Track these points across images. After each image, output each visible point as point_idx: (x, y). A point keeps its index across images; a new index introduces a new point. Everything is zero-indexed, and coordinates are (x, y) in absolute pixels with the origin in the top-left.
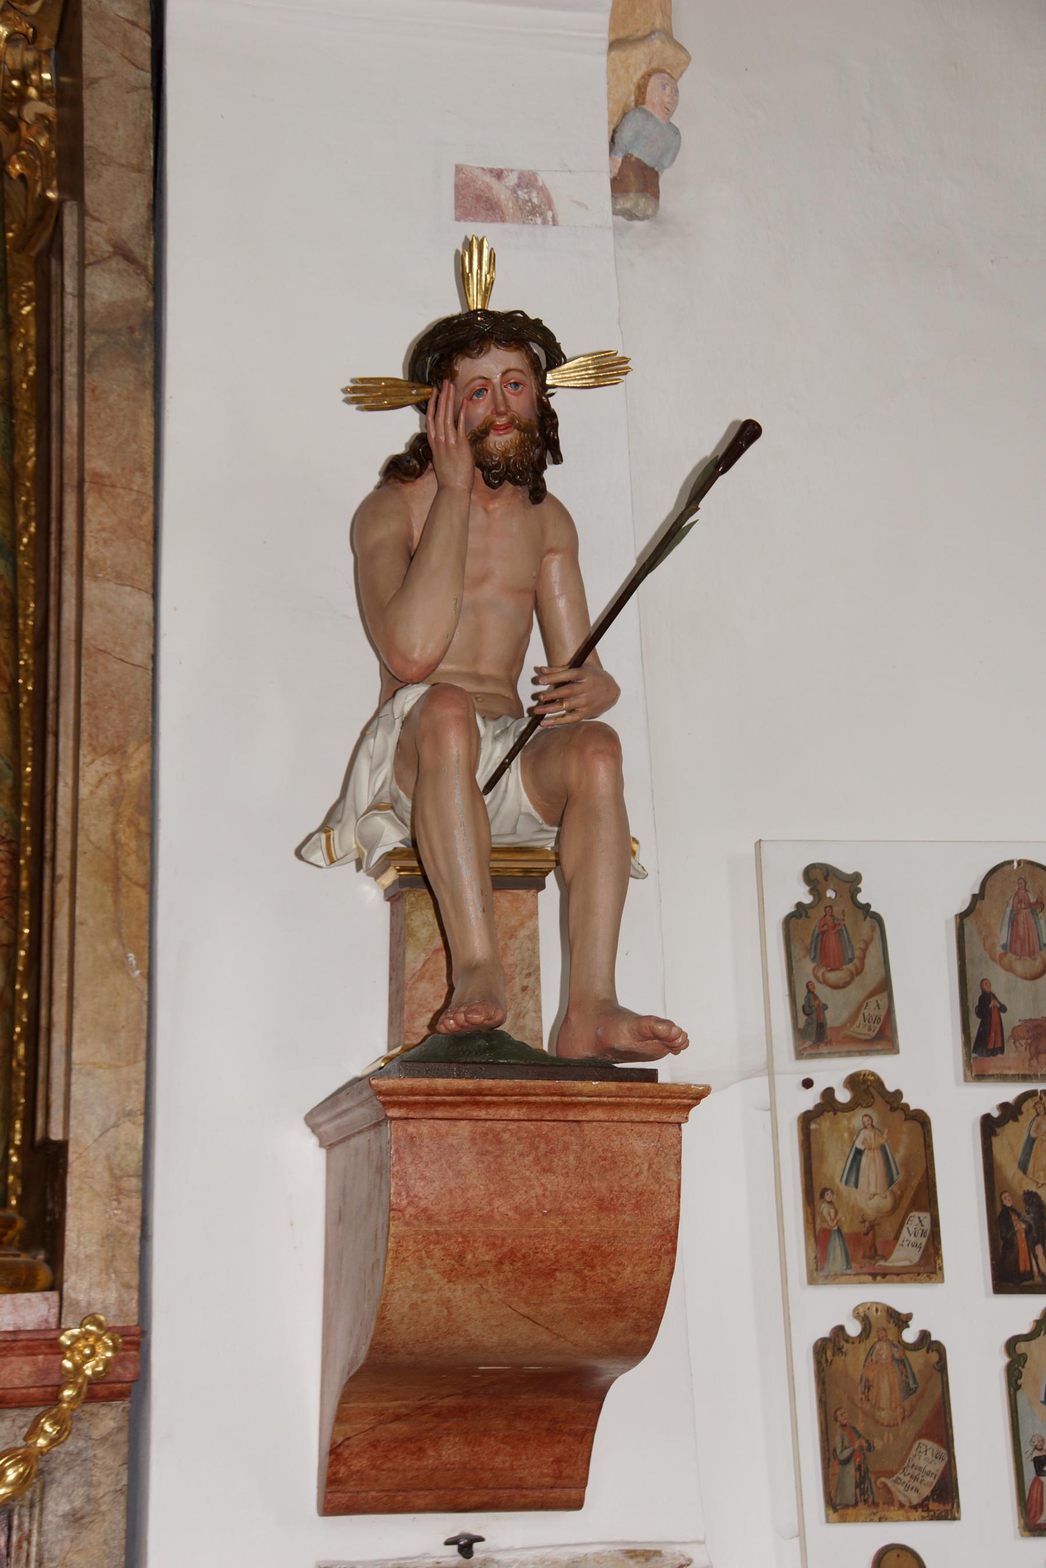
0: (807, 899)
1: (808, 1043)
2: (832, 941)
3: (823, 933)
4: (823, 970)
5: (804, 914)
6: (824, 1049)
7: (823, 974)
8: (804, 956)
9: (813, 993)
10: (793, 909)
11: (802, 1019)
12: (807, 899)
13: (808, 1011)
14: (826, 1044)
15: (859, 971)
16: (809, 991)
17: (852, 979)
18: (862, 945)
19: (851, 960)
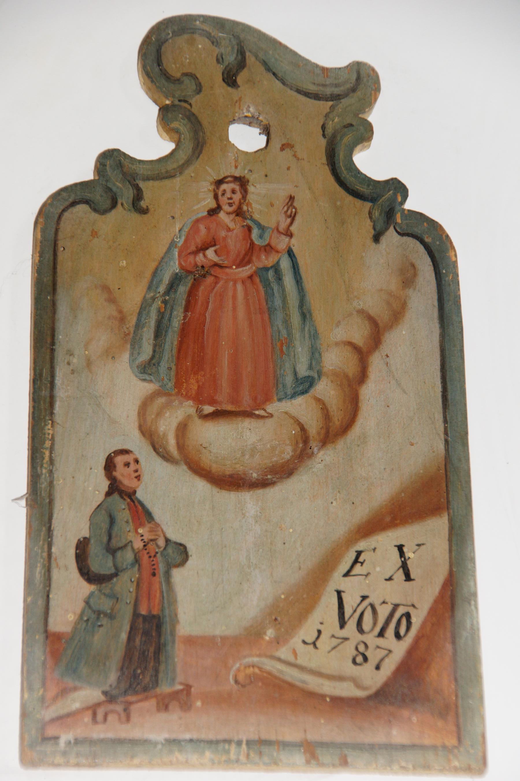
0: (148, 142)
1: (89, 694)
2: (232, 311)
3: (198, 275)
4: (185, 409)
5: (127, 194)
6: (151, 724)
7: (182, 429)
8: (110, 354)
9: (130, 495)
10: (87, 173)
11: (71, 593)
12: (148, 142)
13: (100, 563)
14: (164, 705)
15: (337, 428)
16: (115, 488)
17: (303, 453)
18: (359, 334)
19: (305, 385)
